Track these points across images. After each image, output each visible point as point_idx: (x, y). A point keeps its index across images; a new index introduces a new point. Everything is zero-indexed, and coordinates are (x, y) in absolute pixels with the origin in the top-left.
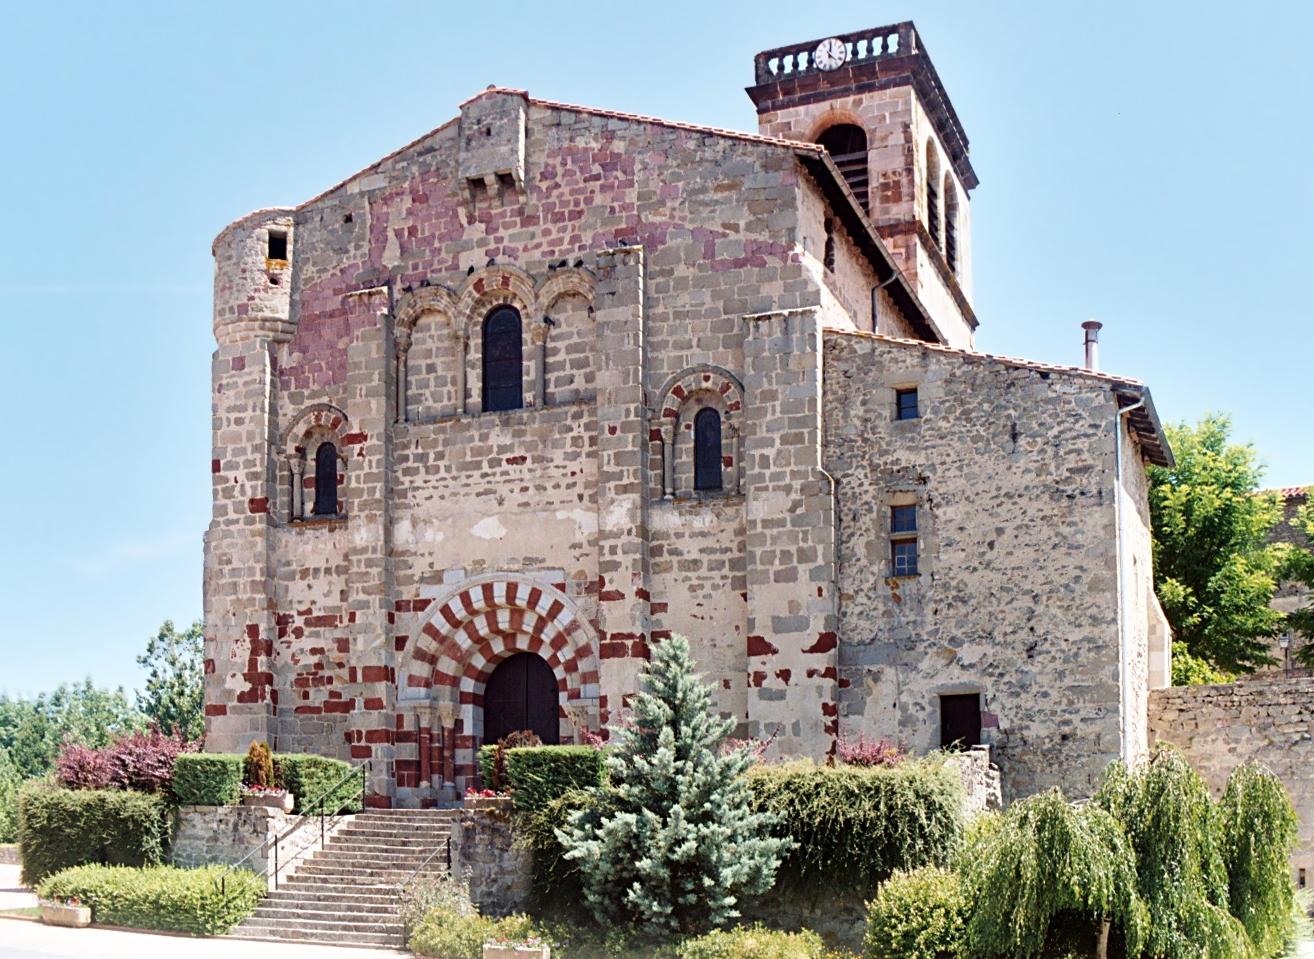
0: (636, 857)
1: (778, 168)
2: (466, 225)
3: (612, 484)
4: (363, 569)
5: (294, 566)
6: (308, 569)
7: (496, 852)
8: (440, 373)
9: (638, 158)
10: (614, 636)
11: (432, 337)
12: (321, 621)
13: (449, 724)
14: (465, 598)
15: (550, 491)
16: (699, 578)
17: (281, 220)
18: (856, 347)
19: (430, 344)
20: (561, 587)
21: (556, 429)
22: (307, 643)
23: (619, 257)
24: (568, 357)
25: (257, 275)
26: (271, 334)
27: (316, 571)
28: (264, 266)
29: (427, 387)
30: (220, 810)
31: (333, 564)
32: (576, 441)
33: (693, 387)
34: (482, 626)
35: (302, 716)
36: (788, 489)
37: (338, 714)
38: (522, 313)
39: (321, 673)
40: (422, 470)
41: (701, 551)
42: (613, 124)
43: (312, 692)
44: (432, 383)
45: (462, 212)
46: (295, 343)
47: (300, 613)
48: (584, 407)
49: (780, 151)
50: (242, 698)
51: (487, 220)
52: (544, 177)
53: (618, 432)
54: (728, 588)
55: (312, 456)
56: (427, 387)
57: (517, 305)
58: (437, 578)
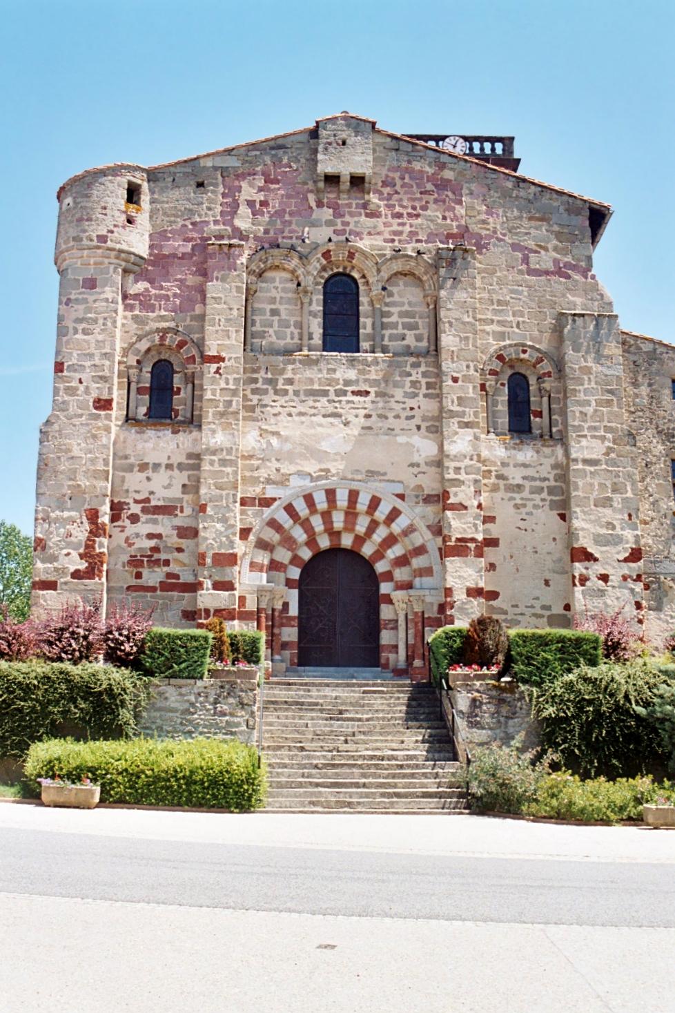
0: (643, 727)
1: (578, 214)
2: (314, 207)
3: (456, 420)
4: (217, 467)
5: (132, 460)
6: (147, 464)
7: (502, 719)
8: (284, 316)
9: (465, 185)
10: (458, 540)
11: (276, 288)
12: (158, 510)
13: (279, 606)
14: (309, 500)
15: (391, 420)
16: (522, 499)
17: (138, 174)
18: (641, 345)
19: (274, 293)
20: (401, 497)
21: (397, 373)
22: (144, 528)
23: (459, 253)
24: (400, 321)
25: (117, 214)
26: (123, 264)
27: (156, 466)
28: (123, 208)
29: (271, 326)
30: (199, 683)
31: (175, 460)
32: (414, 384)
33: (514, 356)
34: (317, 523)
35: (134, 594)
36: (603, 438)
37: (175, 593)
38: (360, 282)
39: (156, 556)
40: (271, 392)
41: (524, 478)
42: (172, 169)
43: (145, 572)
44: (276, 324)
45: (312, 198)
46: (141, 274)
47: (136, 502)
48: (421, 359)
49: (579, 202)
50: (76, 575)
51: (335, 207)
52: (385, 184)
53: (460, 383)
54: (547, 508)
55: (148, 368)
56: (271, 326)
57: (356, 275)
58: (283, 482)
